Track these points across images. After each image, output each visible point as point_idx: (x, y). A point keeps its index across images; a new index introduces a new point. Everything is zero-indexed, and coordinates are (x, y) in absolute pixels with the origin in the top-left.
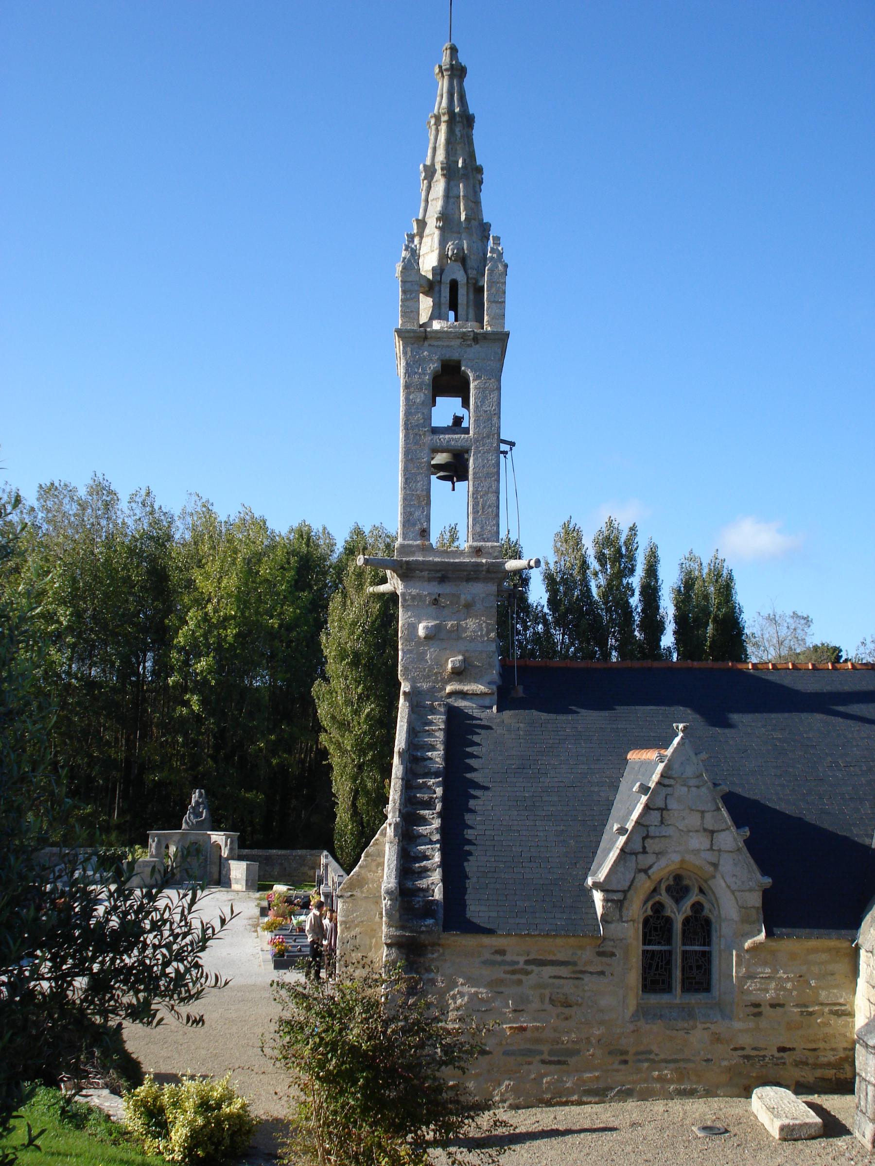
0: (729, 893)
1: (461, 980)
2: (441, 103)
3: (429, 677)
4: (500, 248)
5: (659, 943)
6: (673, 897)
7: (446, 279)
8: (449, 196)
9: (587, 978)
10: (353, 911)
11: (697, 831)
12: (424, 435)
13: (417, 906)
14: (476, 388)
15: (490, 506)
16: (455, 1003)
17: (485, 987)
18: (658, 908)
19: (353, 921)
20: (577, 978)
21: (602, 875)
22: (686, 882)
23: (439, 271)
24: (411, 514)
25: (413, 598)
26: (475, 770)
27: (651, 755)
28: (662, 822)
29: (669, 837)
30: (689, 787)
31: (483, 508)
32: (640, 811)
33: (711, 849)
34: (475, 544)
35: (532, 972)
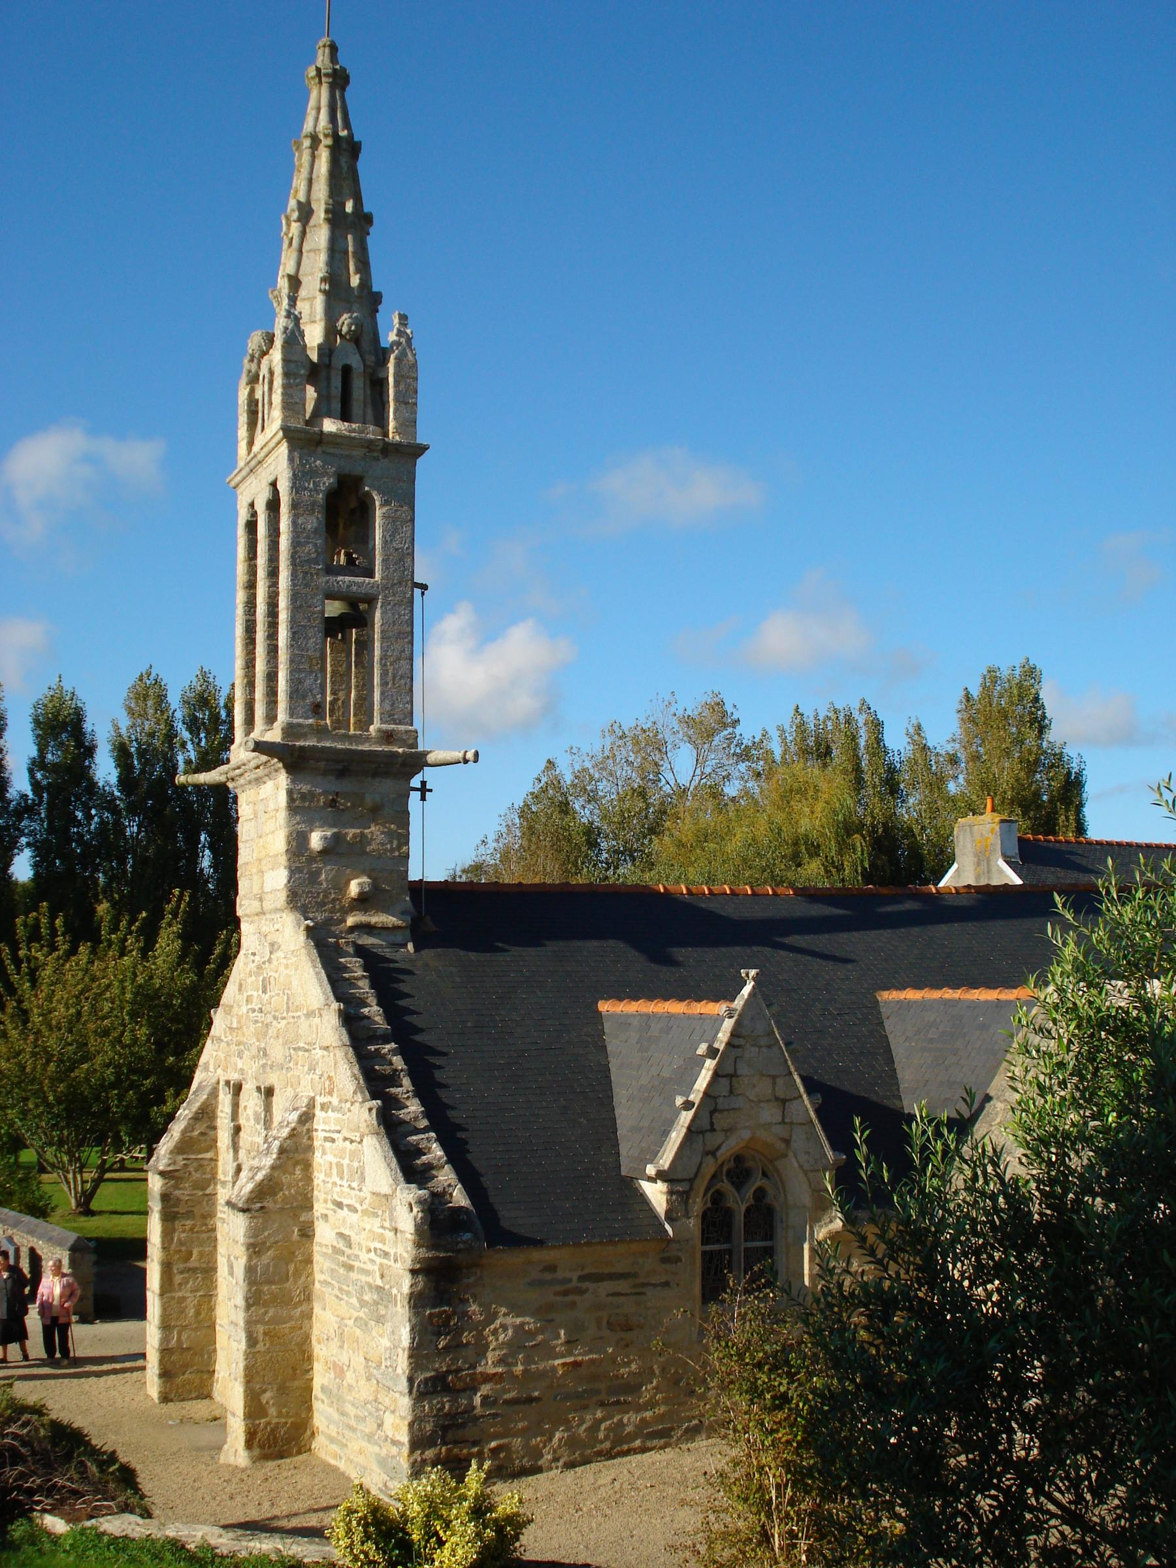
0: (801, 1175)
1: (504, 1310)
2: (317, 119)
3: (324, 904)
4: (408, 331)
5: (718, 1242)
6: (733, 1183)
7: (338, 363)
8: (336, 252)
9: (649, 1292)
10: (264, 1229)
11: (768, 1101)
12: (317, 574)
13: (441, 1217)
14: (384, 516)
15: (402, 677)
16: (497, 1340)
17: (532, 1316)
18: (718, 1198)
19: (264, 1243)
20: (638, 1294)
21: (666, 1159)
22: (750, 1164)
23: (326, 350)
24: (300, 681)
25: (303, 797)
26: (422, 1030)
27: (721, 1008)
28: (731, 1092)
29: (739, 1109)
30: (760, 1047)
31: (394, 679)
32: (708, 1079)
33: (783, 1122)
34: (384, 727)
35: (587, 1290)
